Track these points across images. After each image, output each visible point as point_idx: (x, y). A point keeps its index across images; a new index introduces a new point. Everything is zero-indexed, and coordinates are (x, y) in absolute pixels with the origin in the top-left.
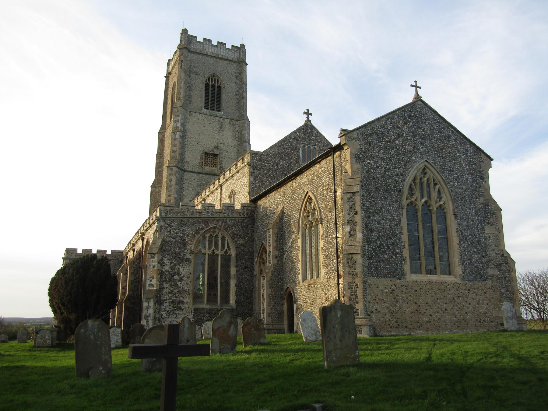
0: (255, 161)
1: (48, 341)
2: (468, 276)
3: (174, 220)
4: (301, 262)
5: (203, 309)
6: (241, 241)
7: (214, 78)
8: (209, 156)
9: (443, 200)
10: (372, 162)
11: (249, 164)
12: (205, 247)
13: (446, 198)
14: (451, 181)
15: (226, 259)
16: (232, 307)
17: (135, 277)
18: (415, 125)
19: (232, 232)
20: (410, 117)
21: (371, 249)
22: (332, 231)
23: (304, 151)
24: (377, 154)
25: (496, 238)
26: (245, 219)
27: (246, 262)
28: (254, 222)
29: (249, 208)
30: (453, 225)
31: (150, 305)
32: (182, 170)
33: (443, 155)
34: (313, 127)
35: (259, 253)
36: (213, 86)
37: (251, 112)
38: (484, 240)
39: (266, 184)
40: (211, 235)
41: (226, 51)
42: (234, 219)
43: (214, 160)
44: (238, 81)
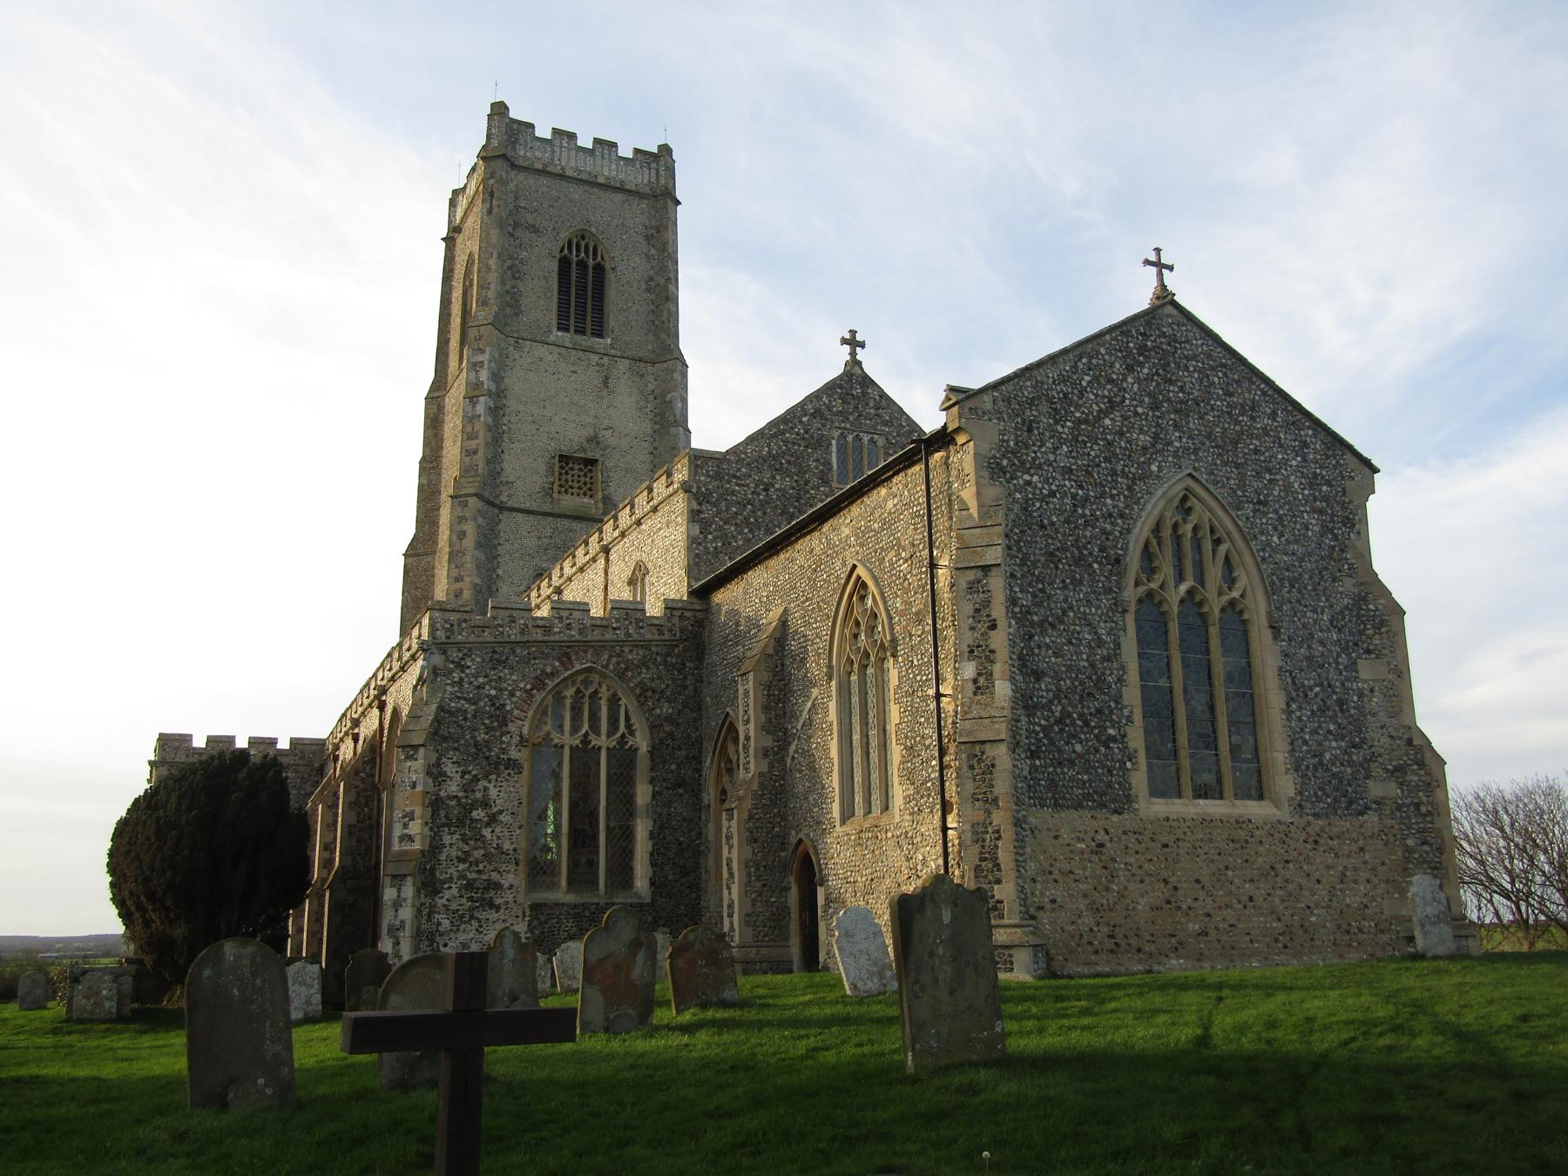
0: (702, 478)
1: (107, 1004)
2: (1313, 803)
3: (470, 650)
5: (557, 904)
6: (666, 709)
7: (583, 244)
8: (571, 465)
10: (1035, 478)
11: (686, 487)
13: (1248, 580)
14: (1262, 533)
15: (623, 760)
16: (640, 897)
17: (358, 814)
18: (1159, 375)
19: (640, 683)
20: (1142, 350)
21: (1038, 728)
22: (924, 678)
23: (842, 449)
24: (1052, 457)
26: (677, 646)
27: (679, 767)
28: (703, 654)
29: (688, 614)
30: (1267, 656)
31: (403, 895)
32: (493, 505)
33: (1238, 457)
34: (867, 382)
36: (582, 264)
38: (1355, 698)
39: (735, 544)
40: (578, 691)
42: (646, 645)
43: (585, 475)
44: (653, 251)
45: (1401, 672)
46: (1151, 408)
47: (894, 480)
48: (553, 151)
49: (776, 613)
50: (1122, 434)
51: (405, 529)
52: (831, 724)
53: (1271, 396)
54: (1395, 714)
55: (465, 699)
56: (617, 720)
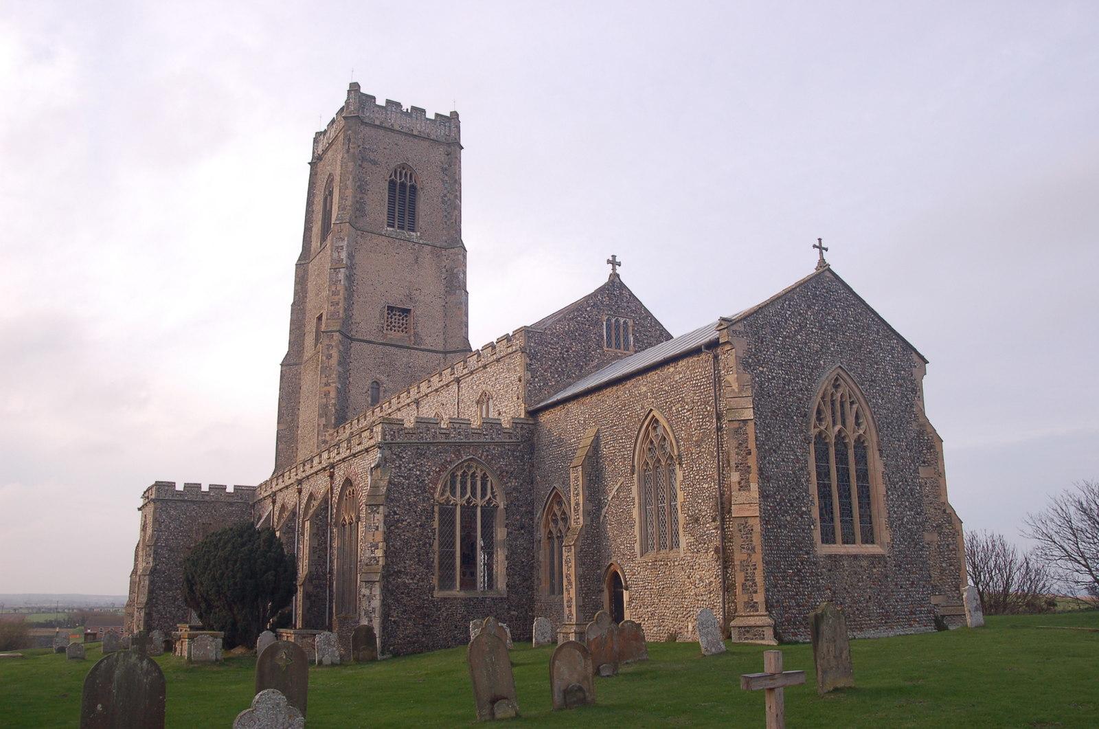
0: (532, 344)
2: (898, 545)
4: (637, 524)
5: (455, 598)
6: (514, 483)
8: (394, 312)
9: (863, 427)
10: (765, 369)
12: (455, 493)
13: (867, 423)
14: (873, 398)
16: (501, 594)
17: (319, 541)
20: (815, 296)
21: (769, 508)
22: (701, 478)
24: (773, 357)
25: (935, 484)
26: (519, 445)
29: (525, 426)
30: (876, 465)
31: (373, 593)
32: (349, 338)
33: (861, 356)
34: (622, 286)
35: (546, 504)
36: (403, 185)
37: (470, 235)
38: (918, 488)
39: (550, 384)
40: (464, 472)
41: (426, 123)
42: (502, 444)
45: (941, 474)
46: (820, 329)
47: (680, 363)
48: (386, 113)
49: (591, 432)
50: (806, 344)
51: (283, 348)
52: (634, 499)
53: (877, 322)
54: (938, 496)
55: (402, 476)
56: (486, 490)
